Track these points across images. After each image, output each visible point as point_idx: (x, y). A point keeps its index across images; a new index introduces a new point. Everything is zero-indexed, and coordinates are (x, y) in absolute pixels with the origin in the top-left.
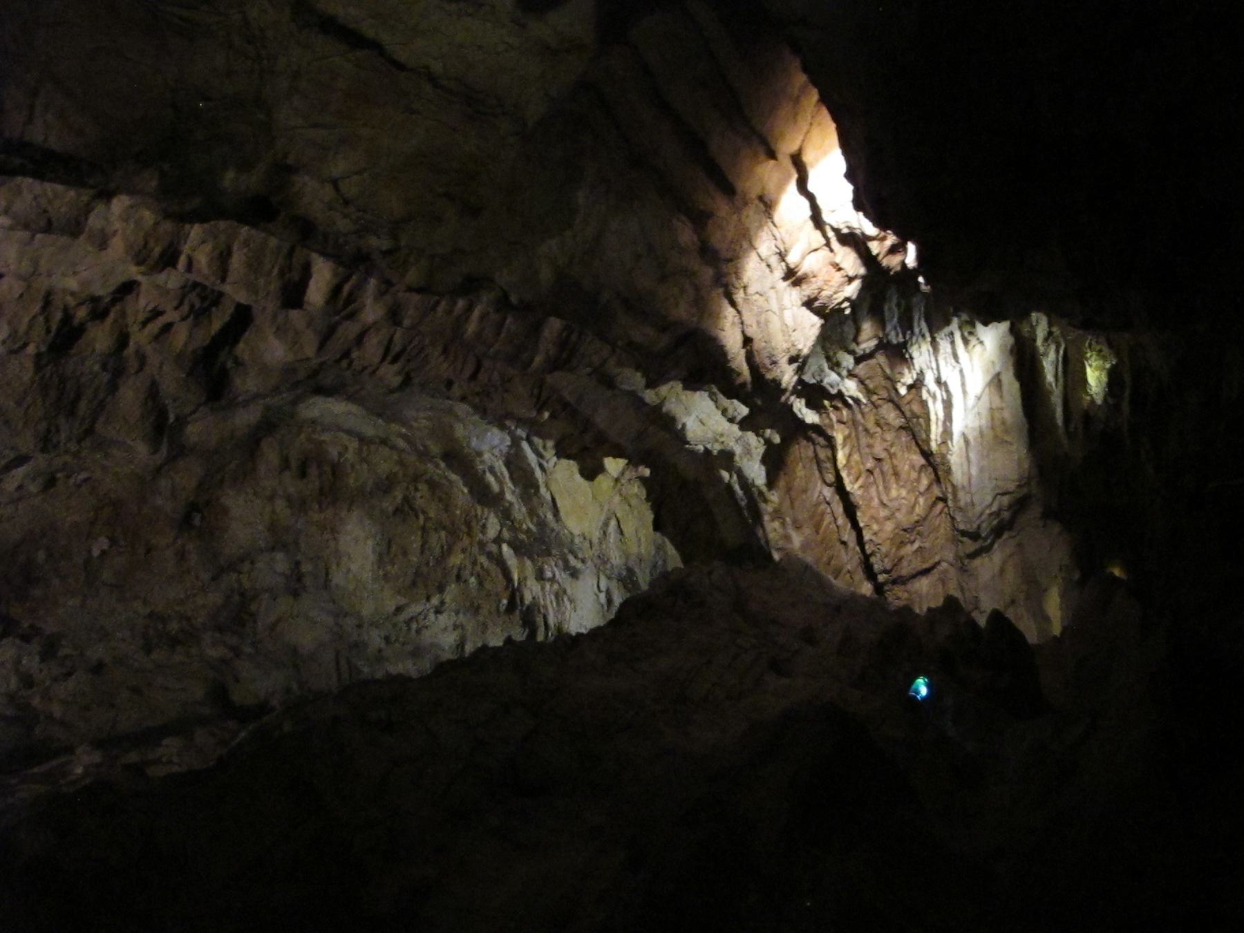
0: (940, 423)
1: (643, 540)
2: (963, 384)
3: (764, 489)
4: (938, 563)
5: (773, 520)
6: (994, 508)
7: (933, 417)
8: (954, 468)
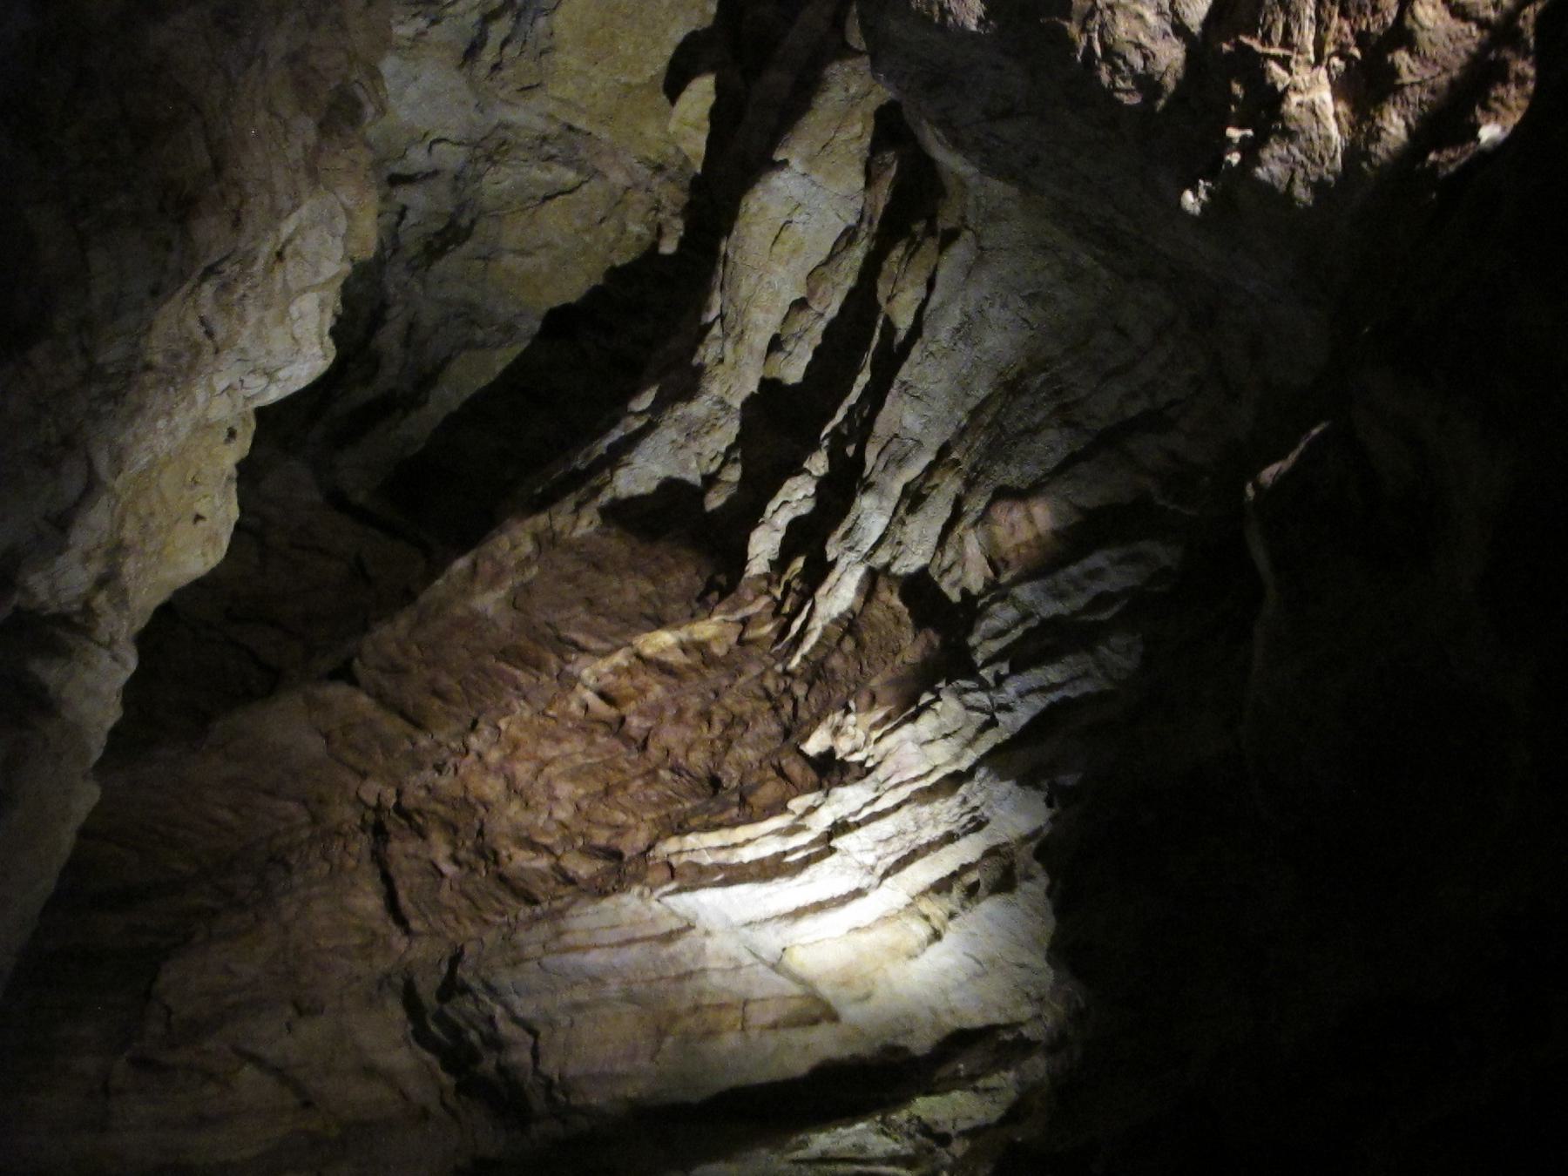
0: (722, 857)
1: (528, 262)
2: (819, 907)
3: (605, 498)
4: (408, 932)
5: (536, 538)
6: (506, 1028)
7: (741, 833)
8: (607, 903)
